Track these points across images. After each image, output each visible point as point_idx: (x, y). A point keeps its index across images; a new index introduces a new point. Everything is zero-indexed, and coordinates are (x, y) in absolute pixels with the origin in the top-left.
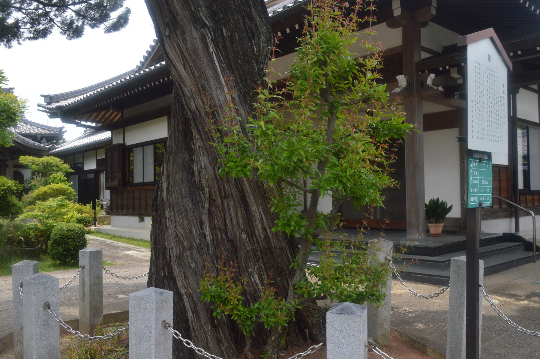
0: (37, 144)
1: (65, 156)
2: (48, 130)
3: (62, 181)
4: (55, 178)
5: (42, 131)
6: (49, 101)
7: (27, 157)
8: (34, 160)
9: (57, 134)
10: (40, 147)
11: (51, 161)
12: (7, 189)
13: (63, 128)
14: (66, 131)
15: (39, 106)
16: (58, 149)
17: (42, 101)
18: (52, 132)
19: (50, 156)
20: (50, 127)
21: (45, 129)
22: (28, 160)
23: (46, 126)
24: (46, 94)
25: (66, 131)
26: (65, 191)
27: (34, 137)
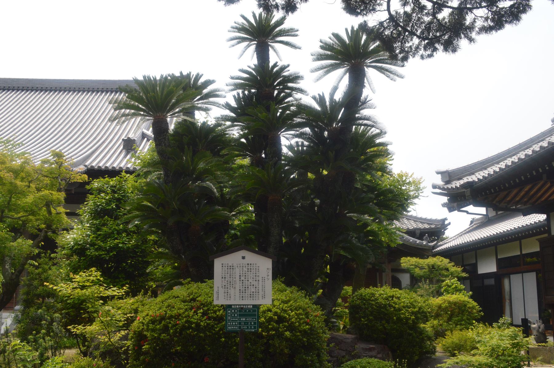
0: (418, 241)
1: (453, 254)
2: (428, 224)
3: (457, 290)
4: (449, 286)
5: (421, 226)
6: (448, 179)
7: (409, 258)
8: (419, 263)
9: (438, 228)
10: (421, 245)
11: (439, 263)
12: (418, 312)
13: (446, 219)
14: (449, 224)
15: (434, 187)
16: (439, 249)
17: (438, 180)
18: (433, 226)
19: (438, 257)
20: (431, 220)
21: (424, 223)
22: (411, 263)
23: (425, 219)
24: (444, 169)
25: (449, 224)
26: (465, 306)
27: (411, 233)
